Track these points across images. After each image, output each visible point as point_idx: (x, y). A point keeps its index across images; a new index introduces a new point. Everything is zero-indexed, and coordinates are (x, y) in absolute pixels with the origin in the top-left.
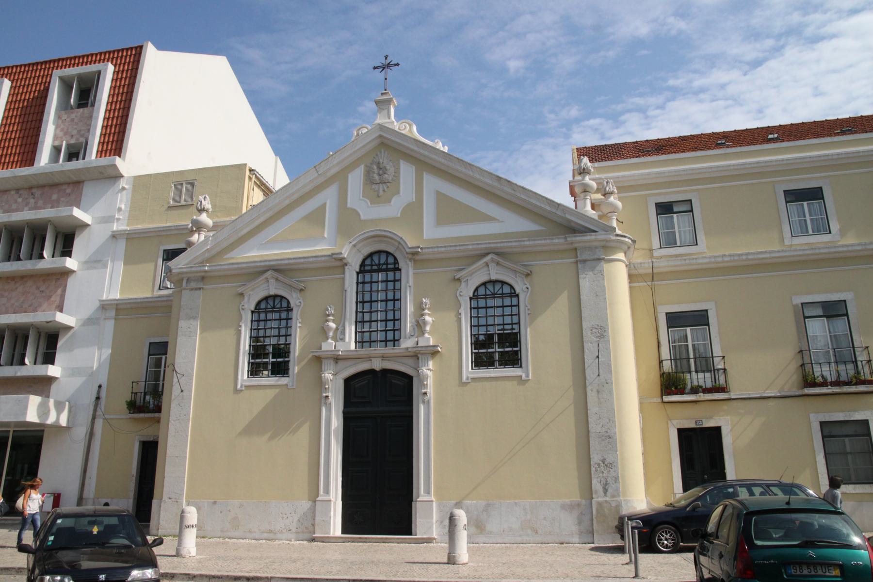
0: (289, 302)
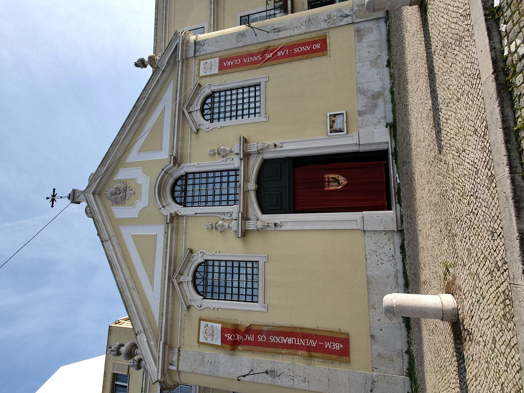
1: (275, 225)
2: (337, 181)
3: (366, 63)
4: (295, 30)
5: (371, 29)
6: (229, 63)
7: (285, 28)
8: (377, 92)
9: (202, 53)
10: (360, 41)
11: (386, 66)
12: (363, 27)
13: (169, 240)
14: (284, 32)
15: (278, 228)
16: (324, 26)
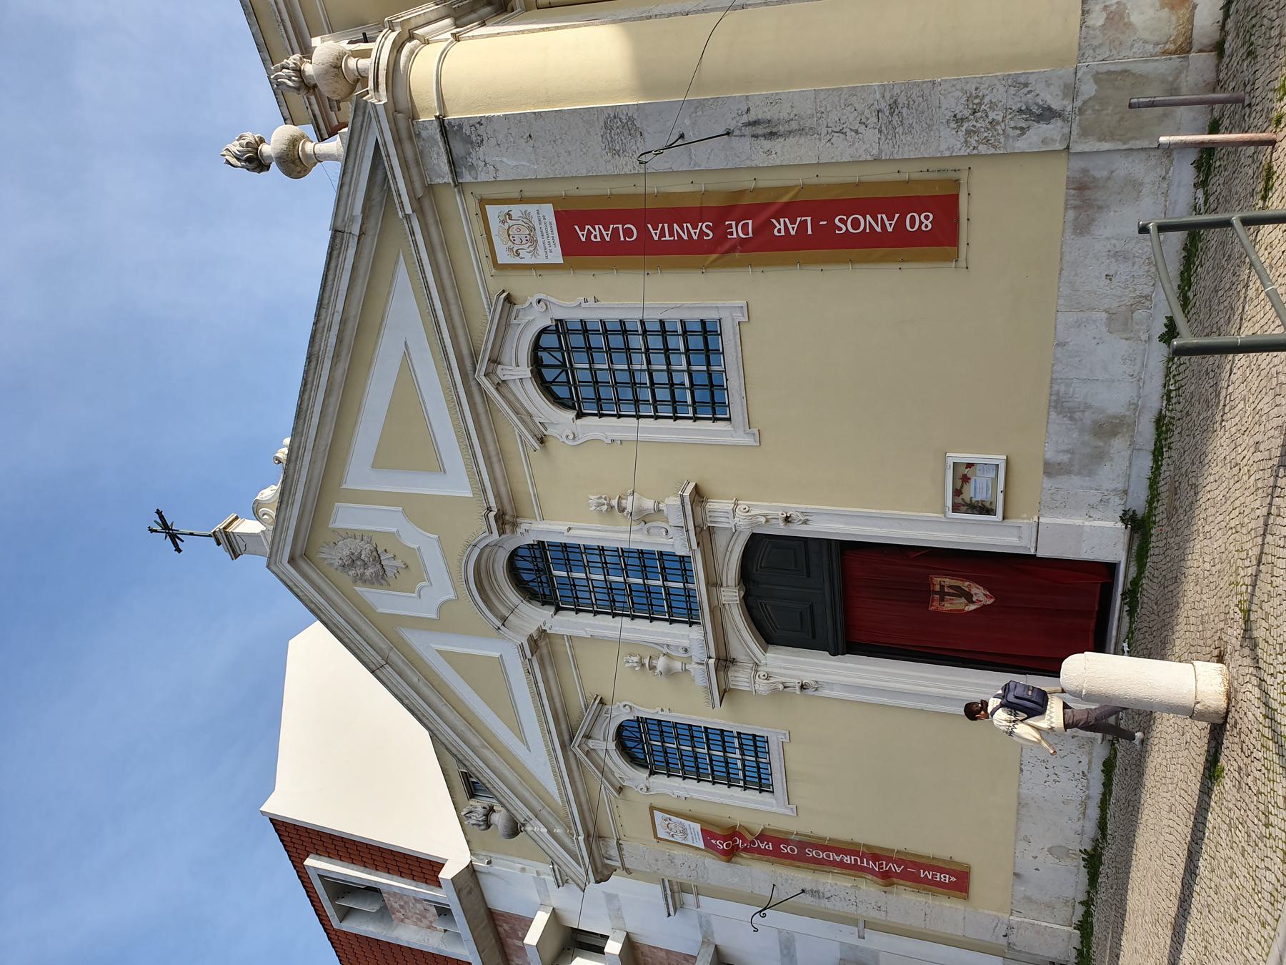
0: (544, 331)
1: (803, 687)
2: (969, 598)
4: (837, 139)
5: (1134, 186)
6: (597, 233)
7: (794, 125)
8: (1115, 417)
9: (482, 177)
10: (1082, 228)
11: (1162, 338)
12: (1105, 173)
14: (791, 140)
15: (810, 692)
16: (949, 142)
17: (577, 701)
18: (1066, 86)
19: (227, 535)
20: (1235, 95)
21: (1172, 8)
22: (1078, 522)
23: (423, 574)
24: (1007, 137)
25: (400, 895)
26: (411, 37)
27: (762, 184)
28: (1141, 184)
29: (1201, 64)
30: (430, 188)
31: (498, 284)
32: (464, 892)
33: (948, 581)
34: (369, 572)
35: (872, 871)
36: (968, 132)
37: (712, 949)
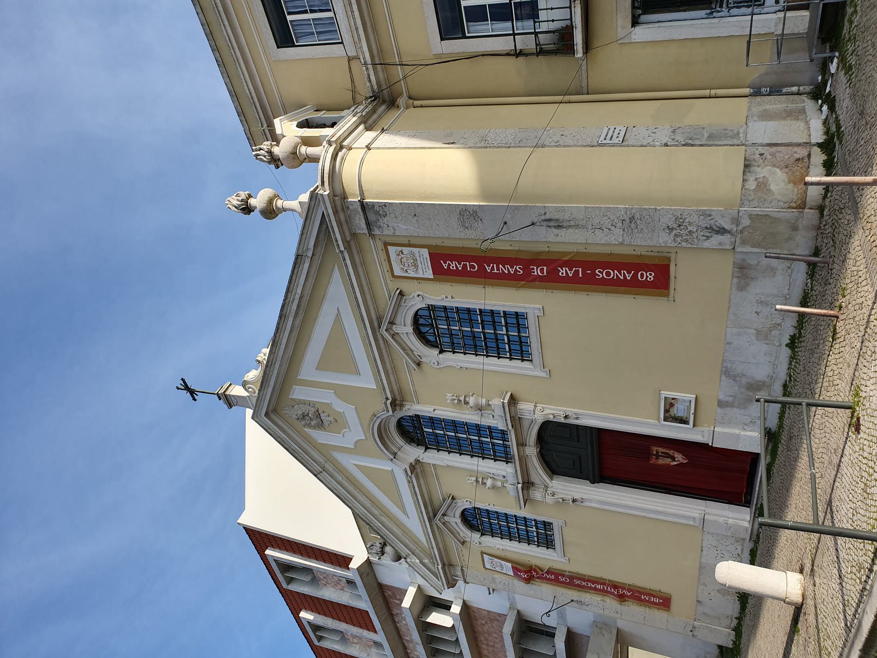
1: (574, 501)
2: (673, 459)
3: (748, 331)
5: (773, 270)
7: (572, 223)
8: (759, 382)
9: (386, 232)
10: (742, 288)
12: (756, 262)
13: (357, 290)
14: (570, 230)
16: (664, 240)
17: (438, 497)
18: (733, 218)
19: (226, 396)
20: (824, 260)
21: (795, 184)
22: (737, 431)
23: (346, 425)
24: (699, 240)
25: (324, 572)
26: (341, 148)
27: (552, 250)
28: (776, 269)
29: (810, 215)
30: (354, 235)
31: (394, 285)
32: (365, 575)
33: (661, 450)
34: (313, 423)
35: (613, 594)
36: (676, 235)
37: (515, 613)
